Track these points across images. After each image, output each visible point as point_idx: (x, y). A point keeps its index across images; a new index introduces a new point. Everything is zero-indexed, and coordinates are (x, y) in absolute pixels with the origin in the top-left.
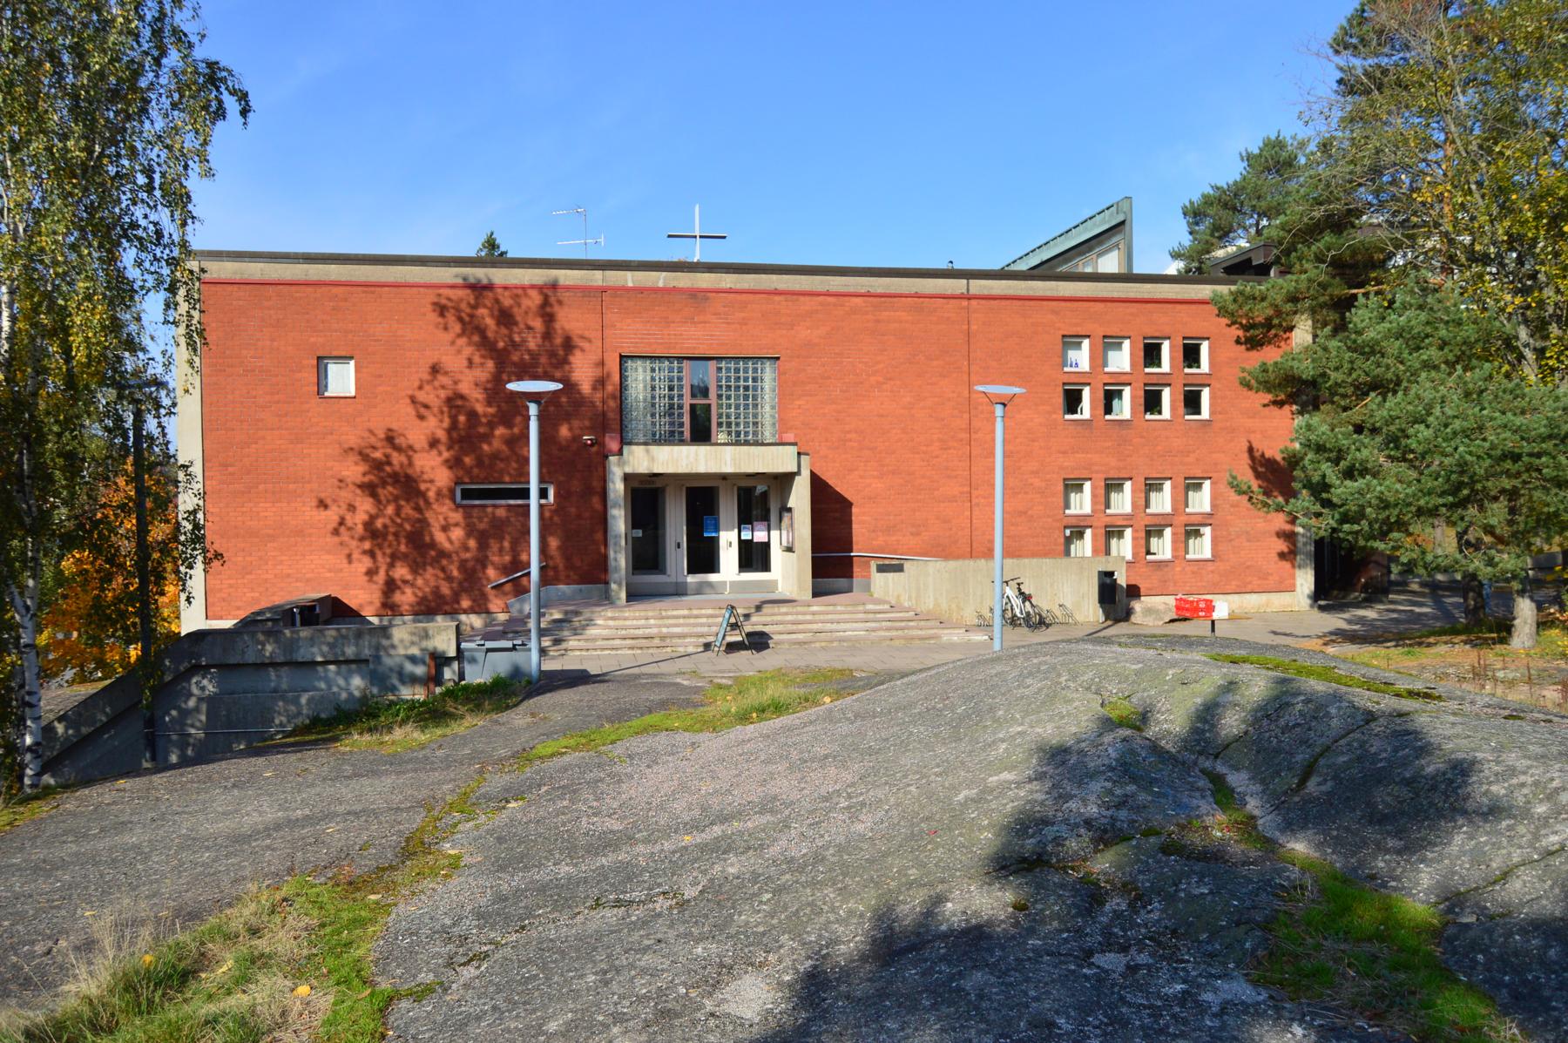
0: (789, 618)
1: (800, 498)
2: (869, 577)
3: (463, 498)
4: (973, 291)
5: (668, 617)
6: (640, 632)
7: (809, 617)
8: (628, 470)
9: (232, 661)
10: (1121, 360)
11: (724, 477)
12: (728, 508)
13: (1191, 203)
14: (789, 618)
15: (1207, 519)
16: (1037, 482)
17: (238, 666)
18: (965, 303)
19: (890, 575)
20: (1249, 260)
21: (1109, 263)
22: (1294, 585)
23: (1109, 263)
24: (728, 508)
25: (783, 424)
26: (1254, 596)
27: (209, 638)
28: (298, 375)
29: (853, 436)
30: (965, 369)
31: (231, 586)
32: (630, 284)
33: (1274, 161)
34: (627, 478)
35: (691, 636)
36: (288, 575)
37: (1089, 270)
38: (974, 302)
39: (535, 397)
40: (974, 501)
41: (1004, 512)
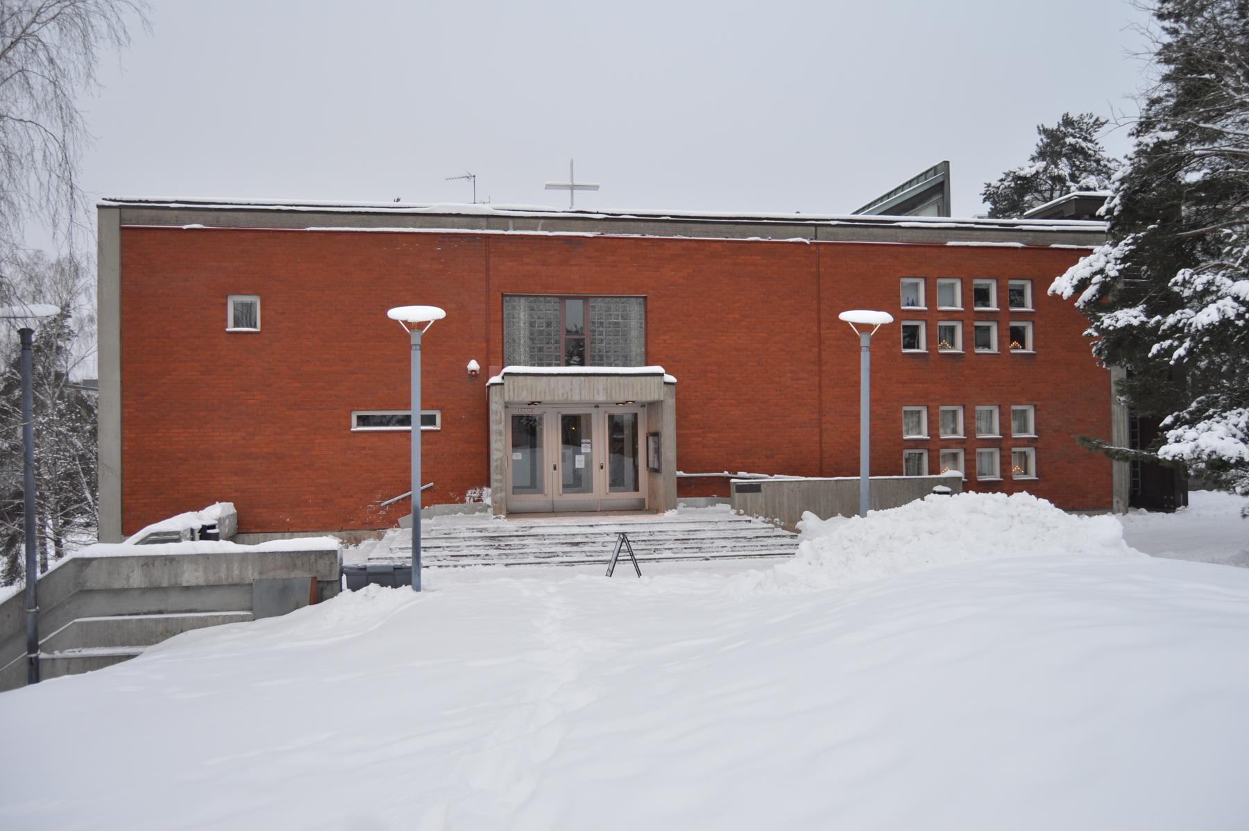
9: (117, 585)
19: (749, 495)
22: (1111, 503)
34: (507, 406)
40: (824, 426)
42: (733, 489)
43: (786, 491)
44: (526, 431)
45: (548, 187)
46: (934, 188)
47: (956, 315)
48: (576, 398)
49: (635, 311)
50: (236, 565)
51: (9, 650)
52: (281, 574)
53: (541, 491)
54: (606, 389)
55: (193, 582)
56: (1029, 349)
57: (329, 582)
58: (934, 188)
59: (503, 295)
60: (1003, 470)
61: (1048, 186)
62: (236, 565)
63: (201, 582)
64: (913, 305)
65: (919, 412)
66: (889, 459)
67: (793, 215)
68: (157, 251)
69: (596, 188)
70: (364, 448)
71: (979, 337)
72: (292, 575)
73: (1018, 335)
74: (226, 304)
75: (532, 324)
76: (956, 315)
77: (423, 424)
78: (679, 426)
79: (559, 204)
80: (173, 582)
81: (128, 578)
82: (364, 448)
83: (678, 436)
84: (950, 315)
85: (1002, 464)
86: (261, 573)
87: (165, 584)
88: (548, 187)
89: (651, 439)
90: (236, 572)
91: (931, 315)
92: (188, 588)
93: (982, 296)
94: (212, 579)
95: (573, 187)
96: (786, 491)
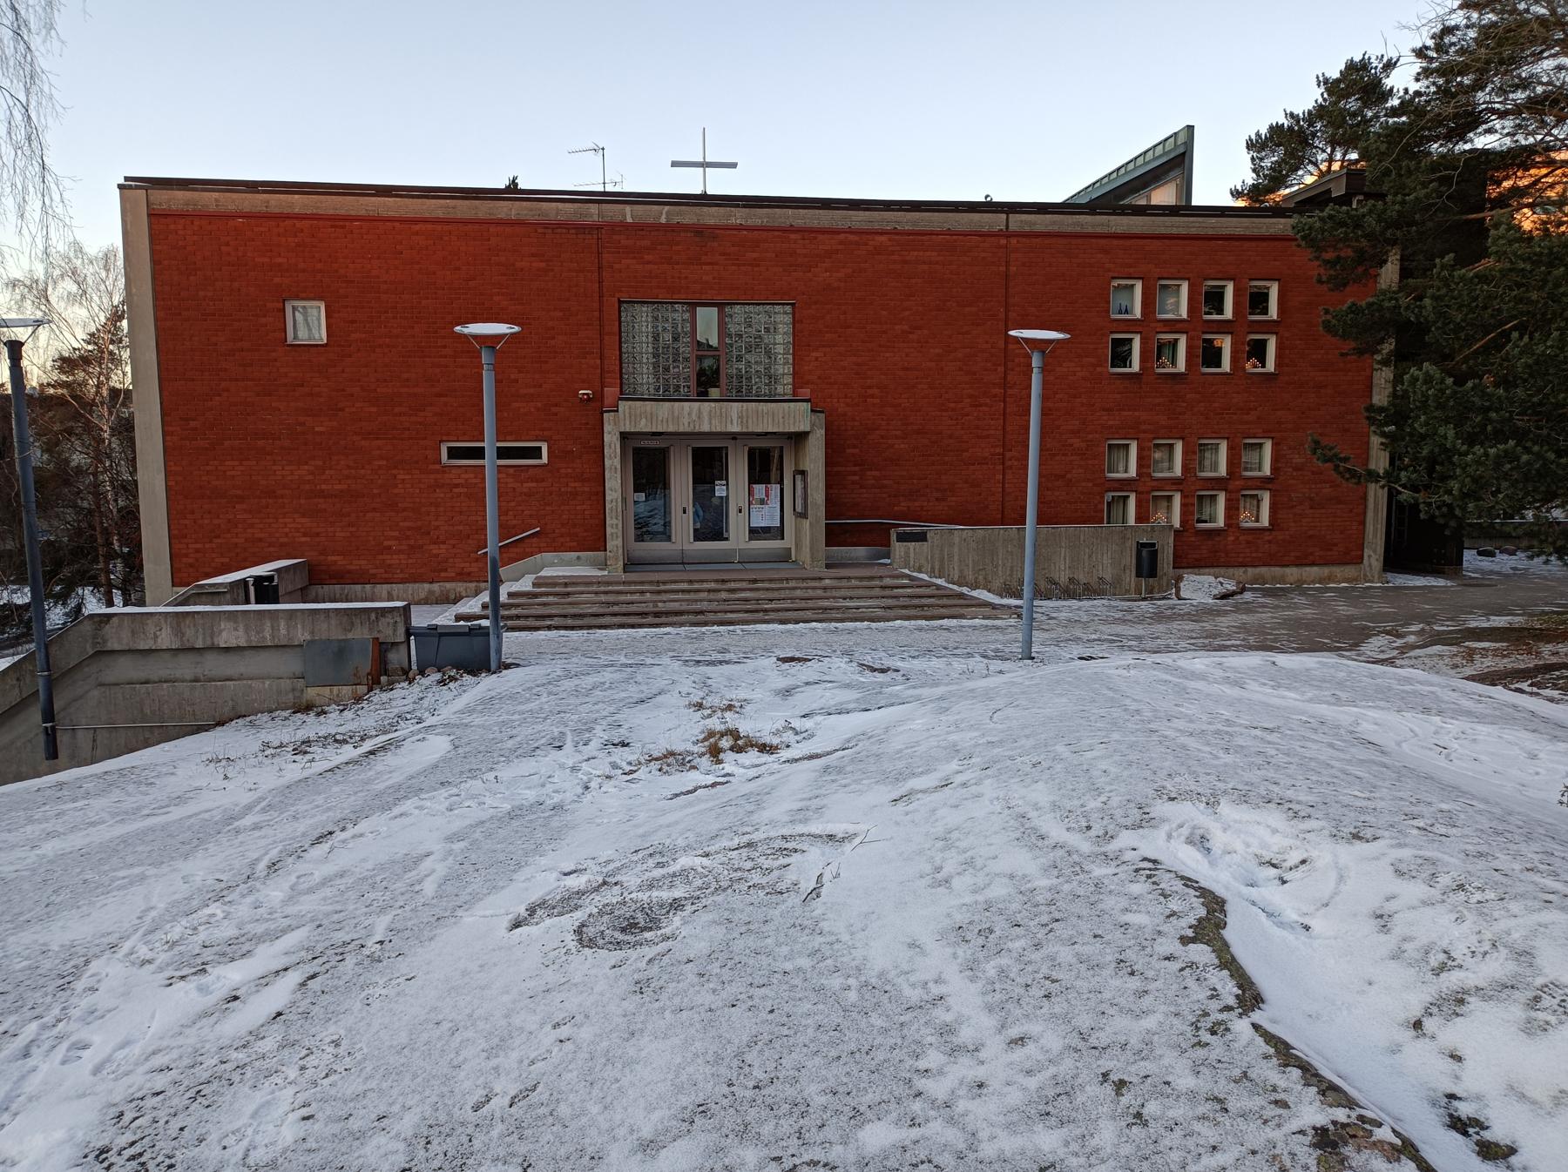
0: (798, 593)
1: (814, 457)
2: (888, 545)
3: (450, 457)
4: (1012, 227)
5: (666, 592)
6: (633, 608)
7: (820, 593)
8: (628, 428)
9: (143, 645)
10: (1179, 304)
11: (734, 436)
12: (738, 469)
13: (1258, 134)
14: (798, 593)
15: (1264, 483)
16: (1077, 443)
17: (151, 651)
18: (1003, 241)
19: (912, 545)
20: (1329, 191)
21: (1163, 196)
22: (1362, 557)
23: (1163, 196)
24: (738, 469)
25: (799, 380)
26: (1315, 569)
27: (115, 619)
28: (263, 320)
29: (876, 391)
30: (1002, 316)
31: (197, 551)
32: (629, 220)
33: (1359, 83)
34: (624, 436)
35: (689, 613)
36: (260, 540)
37: (1143, 202)
38: (1014, 241)
39: (489, 341)
40: (1008, 463)
41: (1041, 475)
42: (894, 537)
43: (957, 540)
44: (648, 464)
45: (675, 164)
46: (1176, 159)
47: (1179, 326)
48: (706, 428)
49: (782, 318)
50: (282, 624)
51: (44, 722)
52: (337, 634)
53: (669, 539)
54: (740, 417)
55: (233, 643)
56: (1271, 366)
57: (393, 644)
58: (1176, 159)
59: (620, 302)
60: (1228, 517)
61: (1325, 156)
62: (282, 624)
63: (243, 643)
64: (1126, 312)
65: (1171, 446)
66: (1077, 501)
67: (979, 198)
68: (199, 243)
69: (734, 165)
70: (457, 486)
71: (1159, 351)
72: (350, 636)
73: (1258, 351)
74: (284, 310)
75: (656, 338)
76: (1179, 326)
77: (499, 457)
78: (829, 463)
79: (689, 183)
80: (208, 643)
81: (156, 637)
82: (457, 486)
83: (827, 474)
84: (1174, 326)
85: (1227, 509)
86: (312, 633)
87: (199, 644)
88: (675, 164)
89: (799, 477)
90: (283, 632)
91: (1149, 322)
92: (227, 649)
93: (1215, 299)
94: (255, 641)
95: (705, 165)
96: (957, 540)
